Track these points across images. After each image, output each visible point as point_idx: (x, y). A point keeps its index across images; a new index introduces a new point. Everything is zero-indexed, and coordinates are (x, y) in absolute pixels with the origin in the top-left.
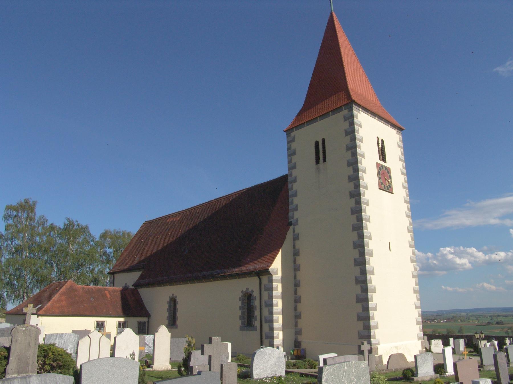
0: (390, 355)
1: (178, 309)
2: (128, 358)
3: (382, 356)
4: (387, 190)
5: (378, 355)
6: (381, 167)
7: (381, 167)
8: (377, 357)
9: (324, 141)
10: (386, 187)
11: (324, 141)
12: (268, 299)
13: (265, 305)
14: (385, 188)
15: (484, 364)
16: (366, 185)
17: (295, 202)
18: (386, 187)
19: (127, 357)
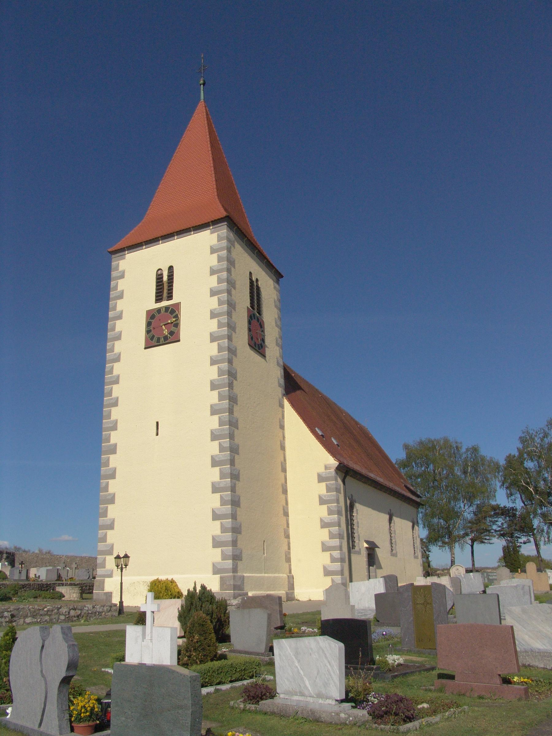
0: (248, 345)
1: (376, 593)
2: (39, 576)
3: (111, 593)
4: (257, 349)
5: (105, 592)
6: (252, 316)
7: (252, 316)
8: (103, 594)
9: (171, 268)
10: (257, 346)
11: (171, 268)
12: (288, 589)
13: (288, 585)
14: (255, 346)
15: (382, 578)
16: (237, 500)
17: (117, 350)
18: (257, 346)
19: (37, 576)
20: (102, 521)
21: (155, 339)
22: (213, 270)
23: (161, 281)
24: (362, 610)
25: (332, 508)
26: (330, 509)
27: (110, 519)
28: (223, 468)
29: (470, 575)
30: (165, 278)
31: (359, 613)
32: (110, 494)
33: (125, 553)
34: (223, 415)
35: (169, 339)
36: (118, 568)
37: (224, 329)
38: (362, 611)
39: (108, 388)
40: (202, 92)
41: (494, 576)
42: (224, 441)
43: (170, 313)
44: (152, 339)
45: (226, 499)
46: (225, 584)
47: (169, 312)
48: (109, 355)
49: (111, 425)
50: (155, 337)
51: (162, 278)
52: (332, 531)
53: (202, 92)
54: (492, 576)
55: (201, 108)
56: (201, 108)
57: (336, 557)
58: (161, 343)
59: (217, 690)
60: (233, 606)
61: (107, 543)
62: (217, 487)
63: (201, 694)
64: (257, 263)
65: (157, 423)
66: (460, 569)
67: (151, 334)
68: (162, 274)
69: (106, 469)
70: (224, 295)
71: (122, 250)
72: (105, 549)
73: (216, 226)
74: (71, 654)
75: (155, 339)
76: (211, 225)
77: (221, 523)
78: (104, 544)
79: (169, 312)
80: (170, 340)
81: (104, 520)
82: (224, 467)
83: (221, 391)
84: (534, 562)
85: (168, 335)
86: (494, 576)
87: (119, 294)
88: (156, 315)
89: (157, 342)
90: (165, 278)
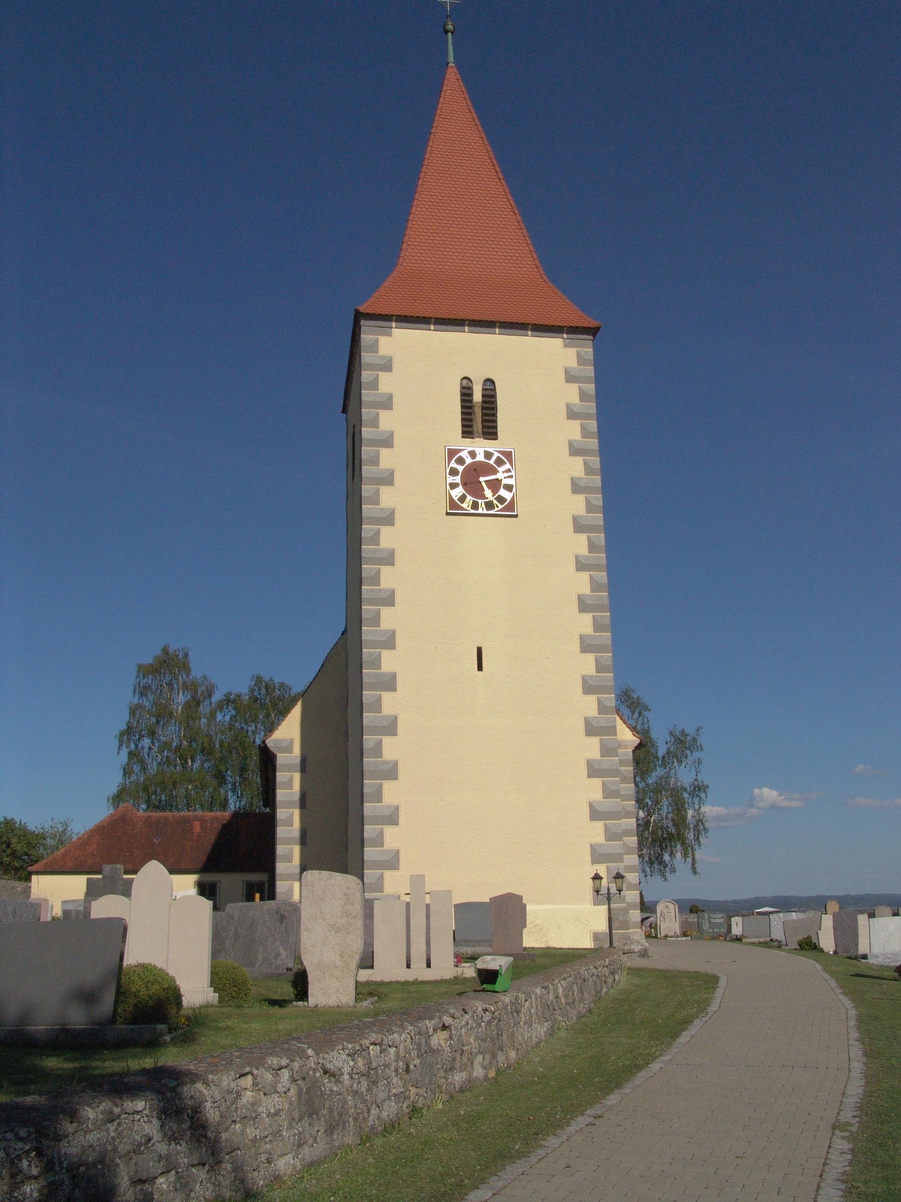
22: (572, 410)
24: (891, 954)
25: (627, 808)
26: (625, 808)
27: (389, 807)
28: (605, 739)
29: (792, 916)
30: (477, 397)
31: (886, 958)
32: (387, 761)
33: (595, 872)
34: (604, 656)
36: (598, 895)
37: (598, 516)
38: (890, 956)
39: (371, 569)
40: (451, 47)
41: (718, 918)
42: (607, 697)
45: (612, 788)
46: (617, 919)
48: (369, 509)
49: (382, 639)
51: (471, 395)
52: (627, 843)
53: (451, 47)
54: (715, 918)
55: (452, 75)
56: (452, 75)
57: (633, 882)
60: (635, 954)
61: (384, 848)
62: (597, 768)
64: (369, 320)
65: (479, 651)
66: (670, 907)
68: (471, 388)
69: (374, 716)
70: (595, 460)
71: (387, 318)
72: (382, 858)
73: (573, 336)
76: (565, 331)
77: (605, 825)
78: (378, 851)
81: (375, 807)
82: (607, 737)
83: (598, 615)
86: (718, 918)
87: (383, 400)
90: (477, 397)
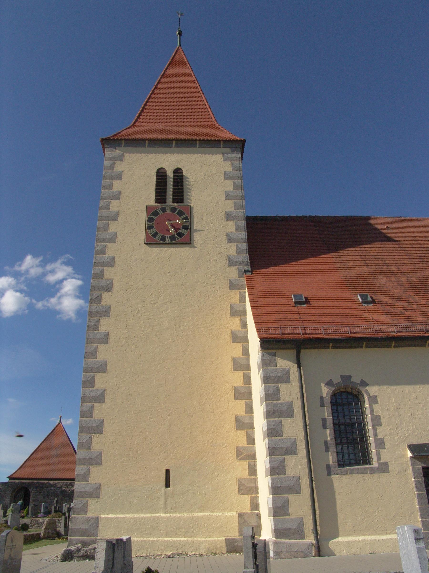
20: (101, 234)
21: (159, 236)
23: (158, 193)
35: (177, 240)
43: (178, 213)
44: (155, 235)
47: (176, 213)
50: (164, 204)
58: (166, 242)
59: (308, 429)
63: (85, 301)
67: (153, 231)
74: (93, 357)
75: (159, 236)
79: (176, 213)
80: (177, 241)
84: (364, 400)
85: (176, 236)
88: (159, 212)
89: (161, 240)
